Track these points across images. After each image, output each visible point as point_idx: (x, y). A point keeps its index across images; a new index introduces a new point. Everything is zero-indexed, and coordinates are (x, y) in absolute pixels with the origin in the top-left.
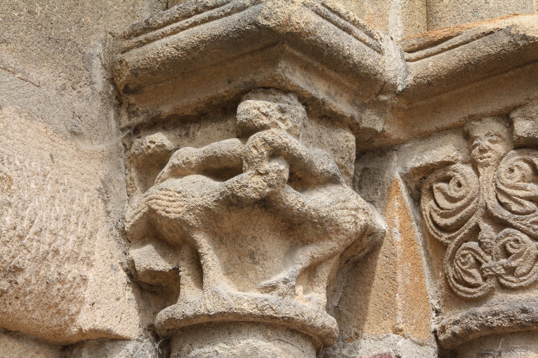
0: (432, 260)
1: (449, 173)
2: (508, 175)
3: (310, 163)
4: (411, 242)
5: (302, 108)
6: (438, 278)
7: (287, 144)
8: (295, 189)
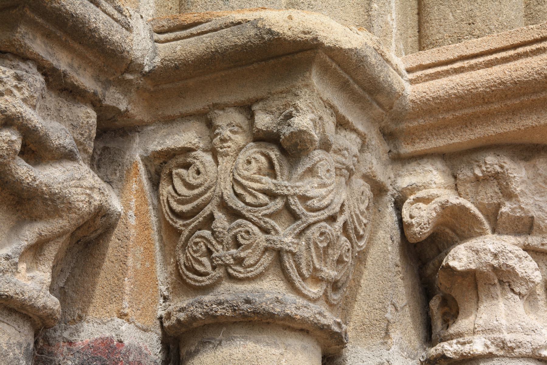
0: (165, 246)
1: (189, 160)
2: (246, 166)
3: (45, 136)
4: (145, 226)
5: (40, 78)
6: (169, 264)
7: (21, 114)
8: (27, 162)
